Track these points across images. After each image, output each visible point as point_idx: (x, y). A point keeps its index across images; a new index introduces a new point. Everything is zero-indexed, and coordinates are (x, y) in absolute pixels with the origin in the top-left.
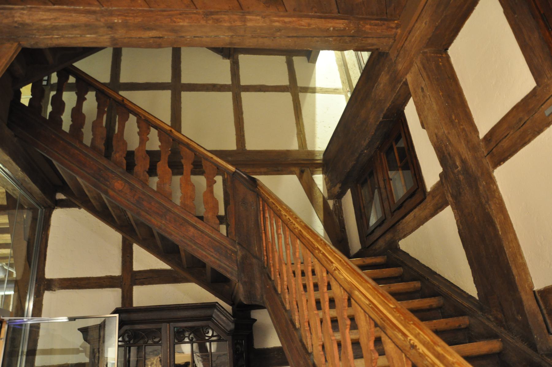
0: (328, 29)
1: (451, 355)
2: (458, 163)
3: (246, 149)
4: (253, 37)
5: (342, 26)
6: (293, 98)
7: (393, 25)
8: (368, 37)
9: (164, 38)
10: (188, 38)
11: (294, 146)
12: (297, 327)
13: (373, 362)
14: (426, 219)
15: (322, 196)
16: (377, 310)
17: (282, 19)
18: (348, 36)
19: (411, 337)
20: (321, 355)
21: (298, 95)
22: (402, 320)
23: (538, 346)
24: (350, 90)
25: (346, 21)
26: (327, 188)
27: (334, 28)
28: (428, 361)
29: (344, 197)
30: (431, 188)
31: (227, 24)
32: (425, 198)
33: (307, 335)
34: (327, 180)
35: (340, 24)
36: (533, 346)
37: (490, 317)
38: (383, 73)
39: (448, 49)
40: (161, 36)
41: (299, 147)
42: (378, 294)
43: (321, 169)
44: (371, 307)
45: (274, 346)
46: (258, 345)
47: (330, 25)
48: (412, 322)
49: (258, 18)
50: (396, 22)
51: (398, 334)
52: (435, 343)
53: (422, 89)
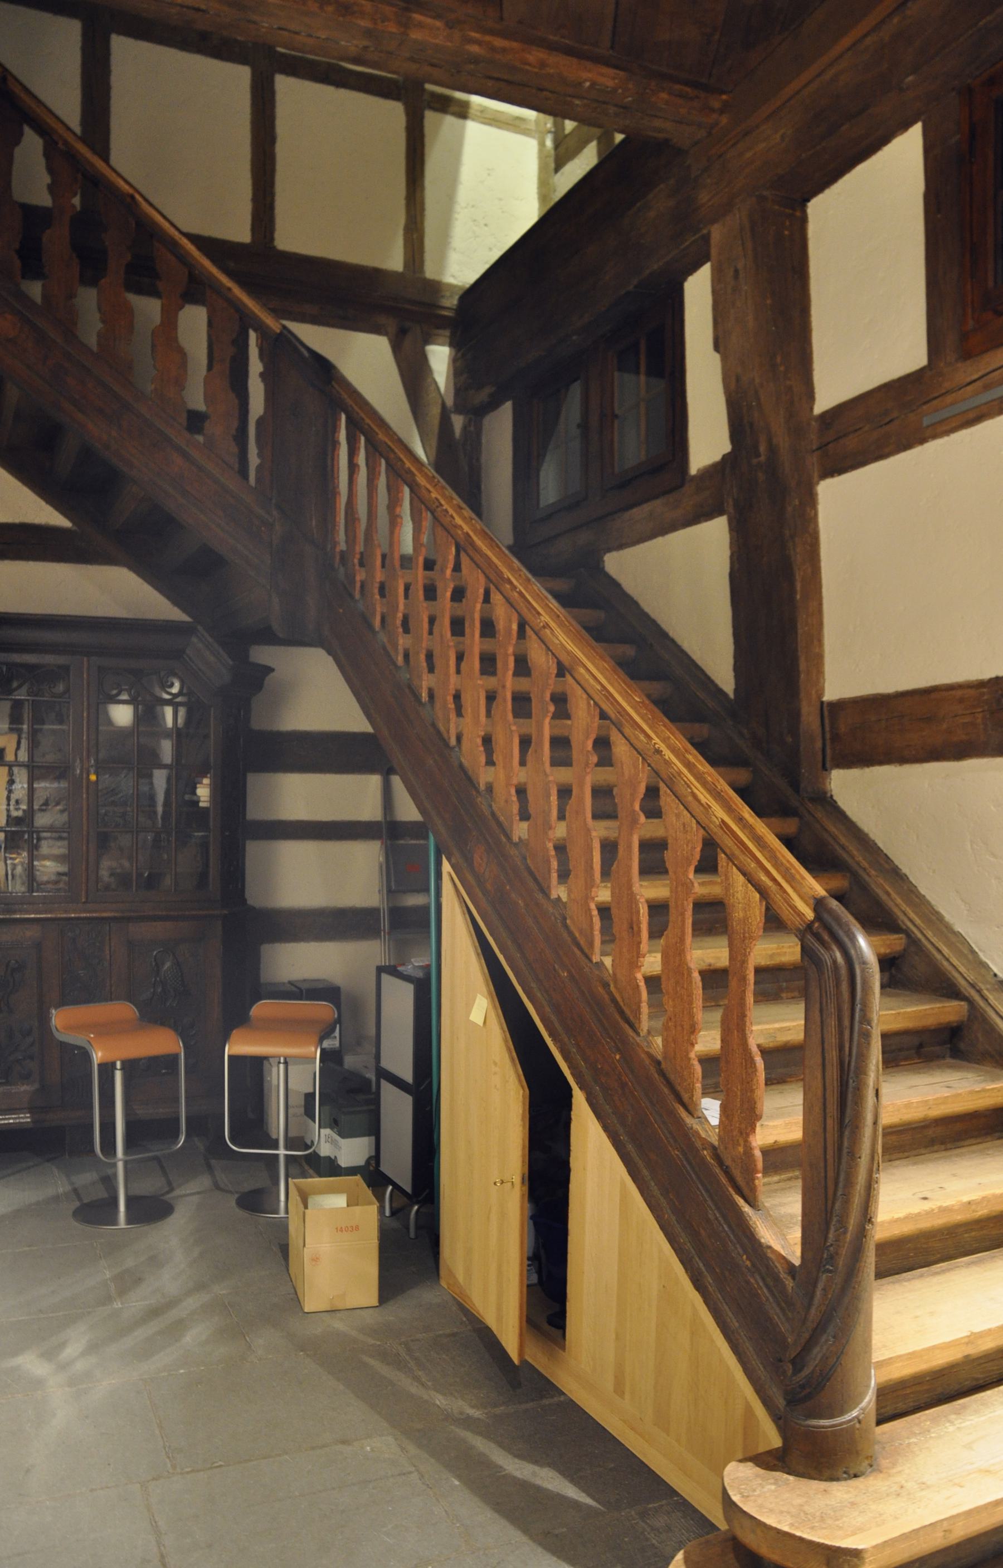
0: (580, 84)
1: (702, 765)
2: (762, 448)
3: (274, 247)
4: (412, 59)
5: (610, 83)
6: (408, 122)
7: (716, 105)
8: (656, 116)
9: (208, 13)
10: (263, 27)
11: (395, 261)
12: (423, 700)
13: (589, 767)
14: (673, 527)
15: (440, 401)
16: (612, 700)
17: (488, 38)
18: (616, 105)
19: (656, 740)
20: (480, 751)
21: (422, 118)
22: (649, 719)
23: (802, 785)
24: (553, 130)
25: (621, 73)
26: (455, 384)
27: (593, 84)
28: (674, 769)
29: (492, 414)
30: (698, 470)
31: (364, 23)
32: (682, 485)
33: (451, 717)
34: (458, 364)
35: (607, 78)
36: (795, 785)
37: (745, 731)
38: (662, 186)
39: (808, 200)
40: (203, 7)
41: (406, 265)
42: (619, 681)
43: (447, 333)
44: (604, 695)
45: (294, 728)
46: (259, 723)
47: (585, 75)
48: (661, 723)
49: (438, 24)
50: (724, 97)
51: (639, 734)
52: (686, 751)
53: (736, 271)
